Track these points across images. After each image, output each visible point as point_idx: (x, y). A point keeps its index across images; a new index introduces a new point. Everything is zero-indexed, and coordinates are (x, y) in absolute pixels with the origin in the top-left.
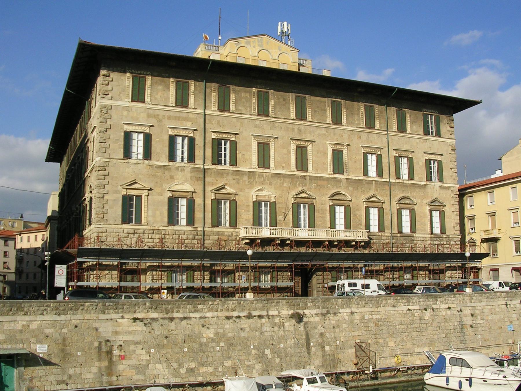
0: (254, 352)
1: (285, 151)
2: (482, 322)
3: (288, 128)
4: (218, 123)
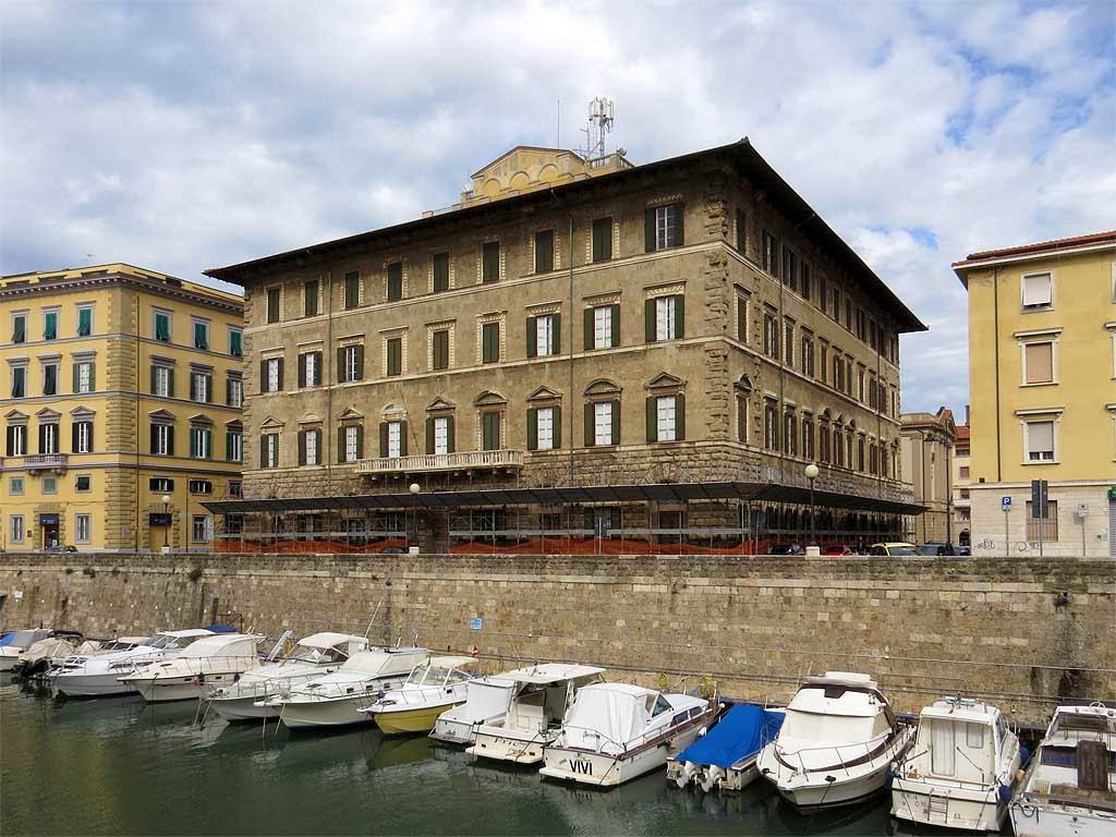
1: (420, 345)
2: (424, 606)
3: (424, 309)
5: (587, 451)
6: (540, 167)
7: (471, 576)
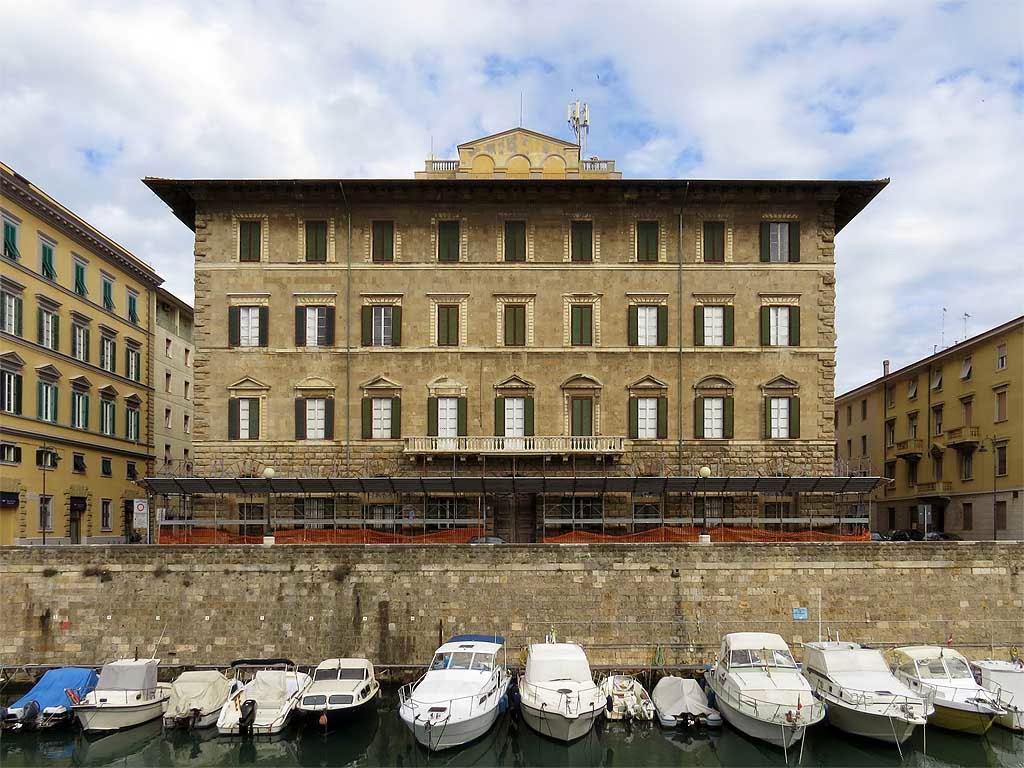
0: (264, 626)
1: (486, 315)
2: (729, 598)
4: (374, 282)
5: (697, 443)
6: (544, 156)
7: (788, 565)
